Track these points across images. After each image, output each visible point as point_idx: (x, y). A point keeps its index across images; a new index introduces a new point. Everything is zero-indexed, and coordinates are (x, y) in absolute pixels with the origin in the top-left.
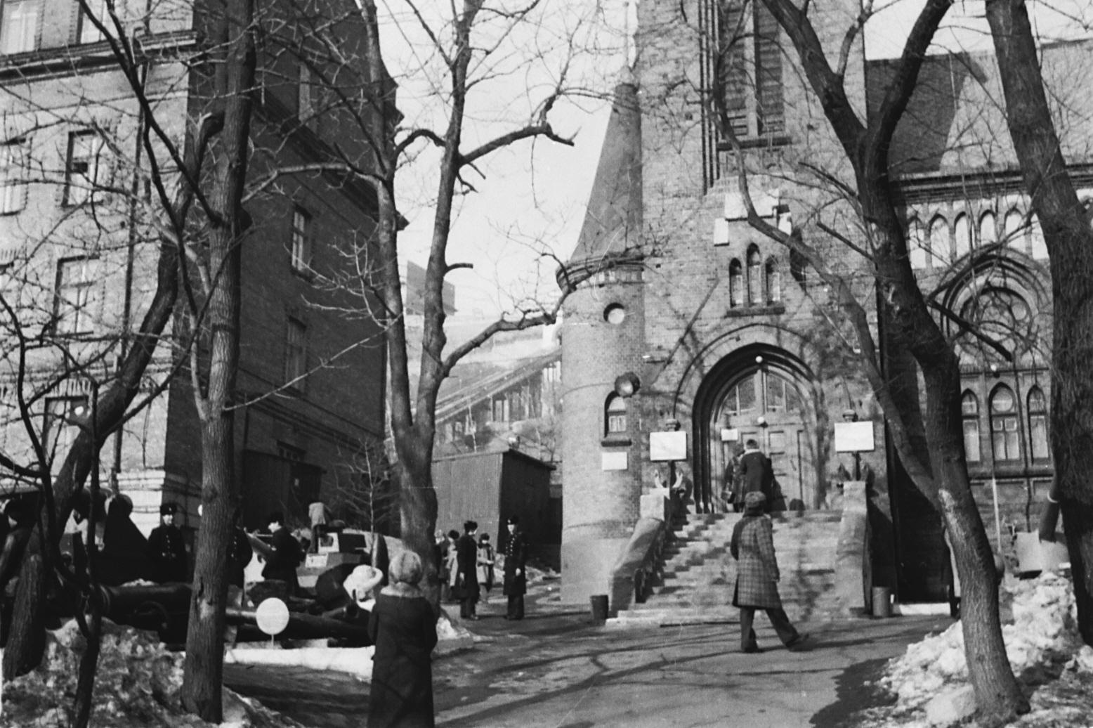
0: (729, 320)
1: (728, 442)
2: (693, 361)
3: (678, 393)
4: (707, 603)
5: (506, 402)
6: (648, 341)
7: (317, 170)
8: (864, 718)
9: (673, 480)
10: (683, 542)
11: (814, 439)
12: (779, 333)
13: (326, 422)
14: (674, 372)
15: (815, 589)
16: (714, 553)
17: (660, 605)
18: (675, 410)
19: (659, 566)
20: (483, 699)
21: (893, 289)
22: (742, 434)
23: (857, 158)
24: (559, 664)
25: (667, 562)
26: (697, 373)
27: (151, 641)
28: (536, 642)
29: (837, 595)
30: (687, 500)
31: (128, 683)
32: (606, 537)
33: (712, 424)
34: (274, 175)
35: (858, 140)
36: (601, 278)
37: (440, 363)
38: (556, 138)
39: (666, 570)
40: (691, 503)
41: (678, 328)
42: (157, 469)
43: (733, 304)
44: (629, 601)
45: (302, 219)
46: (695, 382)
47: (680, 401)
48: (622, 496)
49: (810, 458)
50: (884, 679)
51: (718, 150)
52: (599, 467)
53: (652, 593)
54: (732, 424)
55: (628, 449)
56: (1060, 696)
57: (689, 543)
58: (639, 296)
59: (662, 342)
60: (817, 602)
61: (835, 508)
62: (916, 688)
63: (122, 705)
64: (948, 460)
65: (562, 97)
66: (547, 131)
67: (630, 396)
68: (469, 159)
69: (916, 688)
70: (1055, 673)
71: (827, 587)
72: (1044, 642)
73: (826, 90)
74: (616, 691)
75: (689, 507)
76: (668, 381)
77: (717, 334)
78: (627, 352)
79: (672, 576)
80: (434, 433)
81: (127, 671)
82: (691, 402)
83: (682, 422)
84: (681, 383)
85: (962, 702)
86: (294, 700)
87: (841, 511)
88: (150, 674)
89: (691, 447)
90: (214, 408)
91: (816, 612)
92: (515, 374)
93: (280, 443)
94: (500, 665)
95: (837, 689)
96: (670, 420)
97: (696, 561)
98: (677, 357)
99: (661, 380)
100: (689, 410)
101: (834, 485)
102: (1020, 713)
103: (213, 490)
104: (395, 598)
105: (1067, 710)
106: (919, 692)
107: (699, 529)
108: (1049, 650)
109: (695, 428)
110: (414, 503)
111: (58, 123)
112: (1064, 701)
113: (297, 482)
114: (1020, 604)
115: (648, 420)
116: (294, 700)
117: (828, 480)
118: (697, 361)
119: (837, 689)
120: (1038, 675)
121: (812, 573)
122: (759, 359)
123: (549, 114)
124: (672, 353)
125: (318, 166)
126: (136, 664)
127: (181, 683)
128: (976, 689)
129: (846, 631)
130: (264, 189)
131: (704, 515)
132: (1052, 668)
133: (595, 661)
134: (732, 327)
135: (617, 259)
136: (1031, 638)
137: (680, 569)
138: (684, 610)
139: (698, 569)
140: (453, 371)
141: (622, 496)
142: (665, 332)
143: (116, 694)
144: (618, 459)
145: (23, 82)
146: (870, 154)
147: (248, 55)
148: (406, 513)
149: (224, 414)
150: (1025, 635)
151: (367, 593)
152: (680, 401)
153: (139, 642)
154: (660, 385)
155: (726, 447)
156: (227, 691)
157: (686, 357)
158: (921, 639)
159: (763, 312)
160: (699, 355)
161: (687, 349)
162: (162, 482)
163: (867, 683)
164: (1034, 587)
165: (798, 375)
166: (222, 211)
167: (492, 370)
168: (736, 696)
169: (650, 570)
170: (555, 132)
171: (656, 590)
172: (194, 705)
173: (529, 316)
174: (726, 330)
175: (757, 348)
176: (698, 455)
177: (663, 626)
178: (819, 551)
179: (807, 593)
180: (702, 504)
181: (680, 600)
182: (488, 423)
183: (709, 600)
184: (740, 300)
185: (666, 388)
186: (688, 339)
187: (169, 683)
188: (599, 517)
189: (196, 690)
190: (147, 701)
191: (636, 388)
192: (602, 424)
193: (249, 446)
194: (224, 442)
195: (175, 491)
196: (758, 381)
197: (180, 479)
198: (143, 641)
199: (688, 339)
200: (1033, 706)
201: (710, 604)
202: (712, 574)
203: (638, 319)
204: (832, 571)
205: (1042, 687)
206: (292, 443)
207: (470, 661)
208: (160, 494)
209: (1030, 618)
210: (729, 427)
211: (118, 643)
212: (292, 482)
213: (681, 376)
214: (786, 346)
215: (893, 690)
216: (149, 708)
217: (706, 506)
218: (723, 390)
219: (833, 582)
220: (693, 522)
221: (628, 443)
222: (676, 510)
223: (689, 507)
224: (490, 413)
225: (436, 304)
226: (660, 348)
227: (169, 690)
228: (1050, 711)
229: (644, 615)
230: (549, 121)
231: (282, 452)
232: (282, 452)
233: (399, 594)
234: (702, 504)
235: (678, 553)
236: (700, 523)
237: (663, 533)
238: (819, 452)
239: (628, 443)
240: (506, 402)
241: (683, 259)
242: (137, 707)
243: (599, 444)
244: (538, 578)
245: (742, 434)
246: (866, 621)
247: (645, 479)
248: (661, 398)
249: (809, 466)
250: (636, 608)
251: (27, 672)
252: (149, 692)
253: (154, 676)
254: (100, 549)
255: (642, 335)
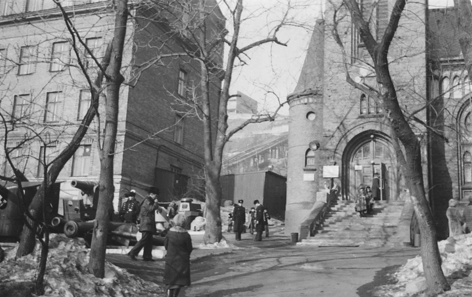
0: (360, 119)
1: (357, 171)
2: (343, 136)
3: (336, 150)
4: (341, 238)
5: (277, 151)
6: (324, 128)
7: (177, 56)
8: (380, 289)
9: (332, 186)
10: (335, 212)
11: (396, 170)
12: (381, 125)
13: (192, 157)
14: (335, 141)
15: (389, 234)
16: (348, 217)
17: (321, 238)
18: (334, 157)
19: (322, 222)
20: (224, 273)
21: (390, 112)
22: (364, 167)
23: (374, 57)
24: (262, 260)
25: (326, 220)
26: (345, 141)
27: (80, 245)
28: (262, 251)
29: (398, 237)
30: (338, 194)
31: (66, 261)
32: (304, 209)
33: (350, 163)
34: (159, 57)
35: (375, 49)
36: (306, 101)
37: (225, 136)
38: (279, 43)
39: (325, 223)
40: (340, 196)
41: (337, 122)
42: (118, 175)
43: (361, 113)
44: (307, 236)
45: (183, 74)
46: (344, 145)
47: (337, 153)
48: (312, 192)
49: (393, 178)
50: (396, 273)
51: (358, 47)
52: (303, 180)
53: (318, 233)
54: (360, 163)
55: (315, 172)
56: (465, 284)
57: (337, 213)
58: (321, 109)
59: (330, 128)
60: (389, 239)
61: (403, 200)
62: (406, 278)
63: (63, 270)
64: (415, 184)
65: (283, 26)
66: (276, 40)
67: (315, 150)
68: (242, 51)
69: (406, 278)
70: (467, 274)
71: (395, 233)
72: (465, 261)
73: (360, 28)
74: (281, 272)
75: (339, 197)
76: (332, 145)
77: (354, 125)
78: (316, 132)
79: (327, 226)
80: (221, 164)
81: (66, 257)
82: (342, 154)
83: (337, 162)
84: (337, 146)
85: (421, 284)
86: (143, 270)
87: (404, 201)
88: (76, 258)
89: (341, 172)
90: (105, 154)
91: (388, 244)
92: (280, 139)
93: (171, 165)
94: (239, 260)
95: (375, 277)
96: (332, 161)
97: (339, 220)
98: (336, 135)
99: (329, 144)
100: (341, 157)
101: (403, 190)
102: (445, 290)
103: (104, 187)
104: (176, 232)
105: (466, 290)
106: (406, 280)
107: (342, 206)
108: (467, 264)
109: (343, 165)
110: (212, 193)
111: (55, 38)
112: (467, 286)
113: (177, 182)
114: (459, 245)
115: (323, 161)
116: (143, 270)
117: (401, 188)
118: (345, 136)
119: (375, 277)
120: (459, 275)
121: (389, 227)
122: (372, 136)
123: (277, 33)
124: (334, 133)
125: (177, 54)
126: (71, 254)
127: (88, 262)
128: (427, 279)
129: (397, 252)
130: (155, 63)
131: (345, 201)
132: (466, 272)
133: (278, 261)
134: (361, 122)
135: (310, 93)
136: (460, 259)
137: (331, 223)
138: (331, 241)
139: (339, 223)
140: (231, 139)
141: (312, 192)
142: (332, 124)
143: (60, 265)
144: (310, 177)
145: (43, 22)
146: (379, 55)
147: (124, 13)
148: (209, 196)
149: (109, 156)
150: (457, 258)
151: (200, 228)
152: (337, 153)
153: (74, 245)
154: (329, 146)
155: (357, 173)
156: (107, 264)
157: (340, 135)
158: (414, 257)
159: (374, 117)
160: (346, 134)
161: (341, 131)
162: (120, 180)
163: (388, 275)
164: (466, 238)
165: (389, 143)
166: (111, 75)
167: (272, 136)
168: (330, 277)
169: (318, 223)
170: (279, 40)
171: (320, 231)
172: (92, 270)
173: (261, 117)
174: (358, 124)
175: (372, 132)
176: (344, 177)
177: (319, 247)
178: (393, 218)
179: (386, 235)
180: (345, 196)
181: (330, 236)
182: (269, 159)
183: (342, 237)
184: (365, 111)
185: (331, 148)
186: (341, 127)
187: (84, 261)
188: (302, 200)
189: (93, 265)
190: (73, 268)
191: (318, 147)
192: (304, 162)
193: (158, 166)
194: (109, 168)
195: (126, 184)
196: (371, 145)
197: (128, 179)
198: (76, 244)
199: (341, 127)
200: (452, 287)
201: (342, 239)
202: (345, 226)
203: (319, 118)
204: (396, 227)
205: (459, 280)
206: (177, 166)
207: (226, 258)
208: (119, 185)
209: (461, 250)
210: (358, 165)
211: (65, 245)
212: (176, 182)
213: (337, 143)
214: (385, 131)
215: (397, 278)
216: (73, 271)
217: (347, 197)
218: (356, 148)
219: (396, 231)
220: (340, 203)
221: (315, 170)
222: (332, 199)
223: (339, 197)
224: (270, 155)
225: (224, 111)
226: (329, 131)
227: (83, 265)
228: (458, 290)
229: (313, 242)
230: (276, 36)
231: (172, 169)
232: (172, 169)
233: (177, 231)
234: (345, 196)
235: (331, 216)
236: (343, 204)
237: (325, 208)
238: (398, 176)
239: (315, 170)
240: (277, 151)
241: (341, 93)
242: (69, 271)
243: (303, 170)
244: (279, 224)
245: (364, 167)
246: (411, 248)
247: (320, 185)
248: (328, 151)
249: (393, 182)
250: (310, 239)
251: (27, 254)
252: (75, 265)
253: (78, 259)
254: (91, 206)
255: (322, 126)
